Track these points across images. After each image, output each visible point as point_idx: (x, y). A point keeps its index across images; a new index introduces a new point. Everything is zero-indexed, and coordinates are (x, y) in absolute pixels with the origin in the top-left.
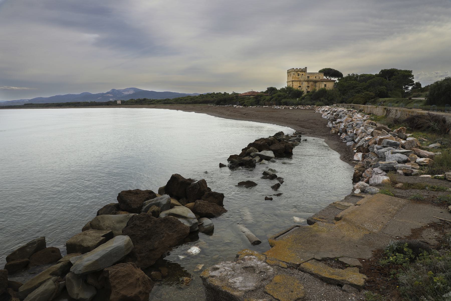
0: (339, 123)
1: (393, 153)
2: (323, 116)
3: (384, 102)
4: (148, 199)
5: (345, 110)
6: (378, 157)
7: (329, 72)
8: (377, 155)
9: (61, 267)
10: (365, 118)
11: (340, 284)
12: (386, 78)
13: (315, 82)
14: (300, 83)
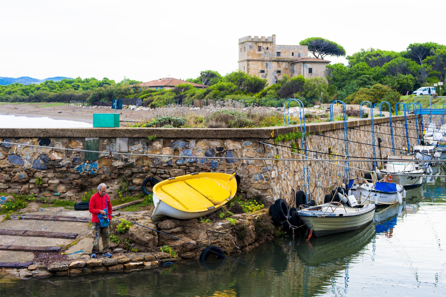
13: (293, 63)
14: (262, 65)
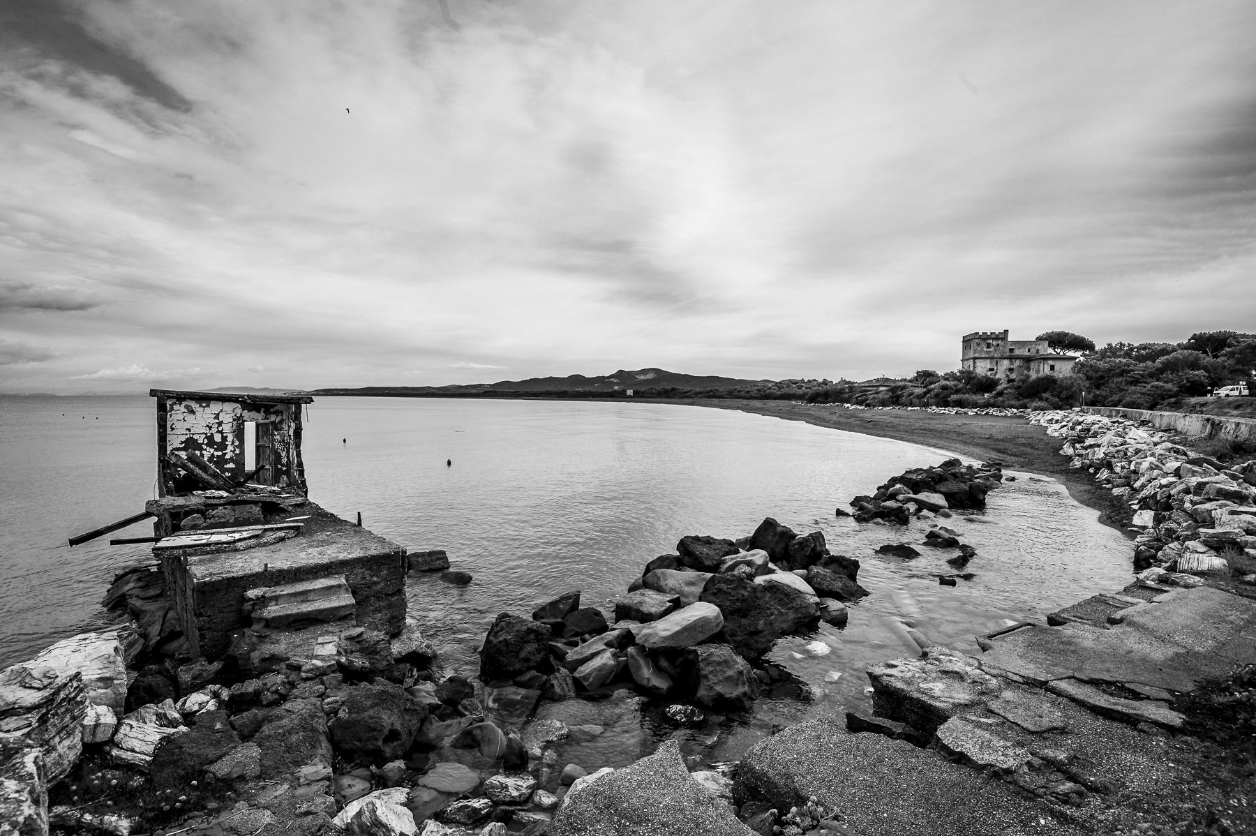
0: (1091, 446)
1: (1233, 513)
2: (1049, 432)
3: (1203, 405)
4: (728, 554)
5: (1105, 420)
6: (1196, 521)
7: (1060, 340)
8: (1192, 516)
9: (618, 637)
10: (1156, 439)
11: (1131, 721)
12: (1205, 352)
13: (1028, 360)
